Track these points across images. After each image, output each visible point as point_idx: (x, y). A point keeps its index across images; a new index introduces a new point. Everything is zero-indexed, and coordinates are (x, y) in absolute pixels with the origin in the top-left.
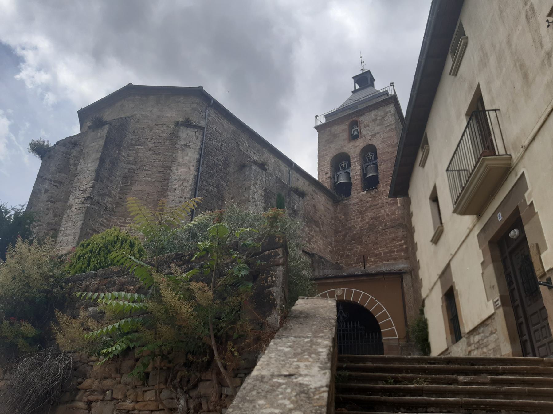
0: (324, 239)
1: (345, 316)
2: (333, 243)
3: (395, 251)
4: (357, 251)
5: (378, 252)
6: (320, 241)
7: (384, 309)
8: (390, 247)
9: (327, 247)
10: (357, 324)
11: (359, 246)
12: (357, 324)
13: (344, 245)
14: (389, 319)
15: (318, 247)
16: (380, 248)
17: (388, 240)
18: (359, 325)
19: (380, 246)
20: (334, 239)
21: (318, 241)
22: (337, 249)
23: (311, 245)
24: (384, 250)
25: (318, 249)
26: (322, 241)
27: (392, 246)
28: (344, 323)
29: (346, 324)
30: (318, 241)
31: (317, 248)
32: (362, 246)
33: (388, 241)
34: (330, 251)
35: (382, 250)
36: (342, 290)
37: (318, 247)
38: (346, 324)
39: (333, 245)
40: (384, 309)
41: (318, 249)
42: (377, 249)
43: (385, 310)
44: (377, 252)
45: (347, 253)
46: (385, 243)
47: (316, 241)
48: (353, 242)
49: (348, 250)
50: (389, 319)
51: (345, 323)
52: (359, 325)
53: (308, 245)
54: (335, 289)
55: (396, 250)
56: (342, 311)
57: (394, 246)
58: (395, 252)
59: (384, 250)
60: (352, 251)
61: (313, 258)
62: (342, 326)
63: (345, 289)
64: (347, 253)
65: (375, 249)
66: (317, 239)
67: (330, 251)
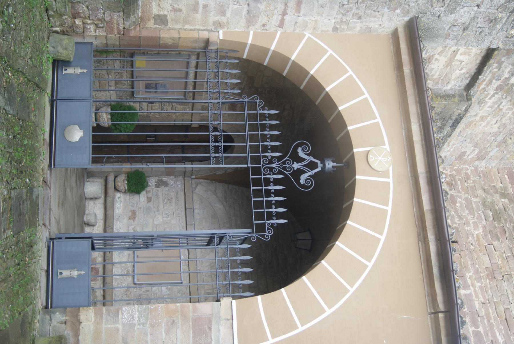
0: (500, 138)
1: (303, 178)
2: (483, 163)
3: (477, 327)
4: (467, 223)
5: (469, 281)
6: (497, 125)
7: (330, 308)
8: (488, 315)
9: (476, 145)
10: (279, 216)
11: (481, 230)
12: (279, 216)
13: (480, 192)
14: (347, 75)
15: (482, 119)
16: (481, 288)
17: (506, 310)
18: (275, 221)
19: (486, 285)
20: (493, 165)
21: (498, 118)
22: (466, 174)
23: (492, 93)
24: (477, 296)
25: (477, 118)
26: (495, 129)
27: (488, 321)
28: (280, 173)
29: (276, 182)
30: (498, 118)
31: (481, 113)
32: (481, 239)
33: (501, 308)
34: (465, 153)
35: (475, 290)
36: (388, 170)
37: (482, 119)
38: (276, 182)
39: (477, 163)
40: (330, 308)
41: (477, 118)
42: (479, 279)
43: (329, 312)
44: (470, 277)
45: (459, 200)
46: (495, 300)
47: (501, 110)
48: (491, 214)
49: (466, 199)
50: (347, 75)
51: (280, 176)
52: (275, 221)
53: (496, 84)
54: (387, 147)
55: (481, 329)
56: (319, 169)
57: (491, 325)
58: (473, 328)
59: (477, 296)
60: (467, 212)
61: (456, 99)
62: (271, 169)
63: (390, 180)
64: (459, 200)
65: (477, 272)
66: (504, 115)
67: (465, 153)
